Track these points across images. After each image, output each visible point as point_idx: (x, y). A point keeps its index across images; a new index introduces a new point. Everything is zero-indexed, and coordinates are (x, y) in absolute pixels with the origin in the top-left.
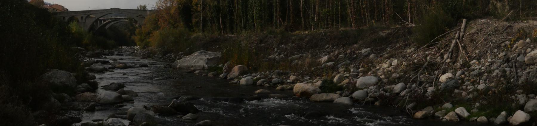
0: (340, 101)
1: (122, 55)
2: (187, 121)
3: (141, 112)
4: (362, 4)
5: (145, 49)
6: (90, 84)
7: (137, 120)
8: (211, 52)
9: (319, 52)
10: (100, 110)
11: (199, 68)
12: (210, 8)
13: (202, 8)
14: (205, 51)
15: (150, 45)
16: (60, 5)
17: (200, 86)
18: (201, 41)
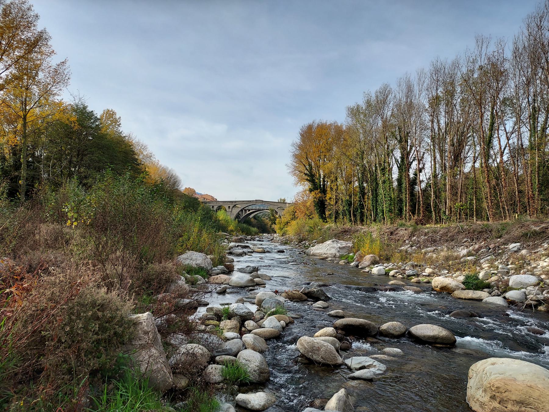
0: (491, 301)
1: (263, 241)
2: (316, 308)
3: (271, 297)
4: (500, 198)
7: (266, 306)
9: (456, 246)
10: (231, 293)
12: (342, 202)
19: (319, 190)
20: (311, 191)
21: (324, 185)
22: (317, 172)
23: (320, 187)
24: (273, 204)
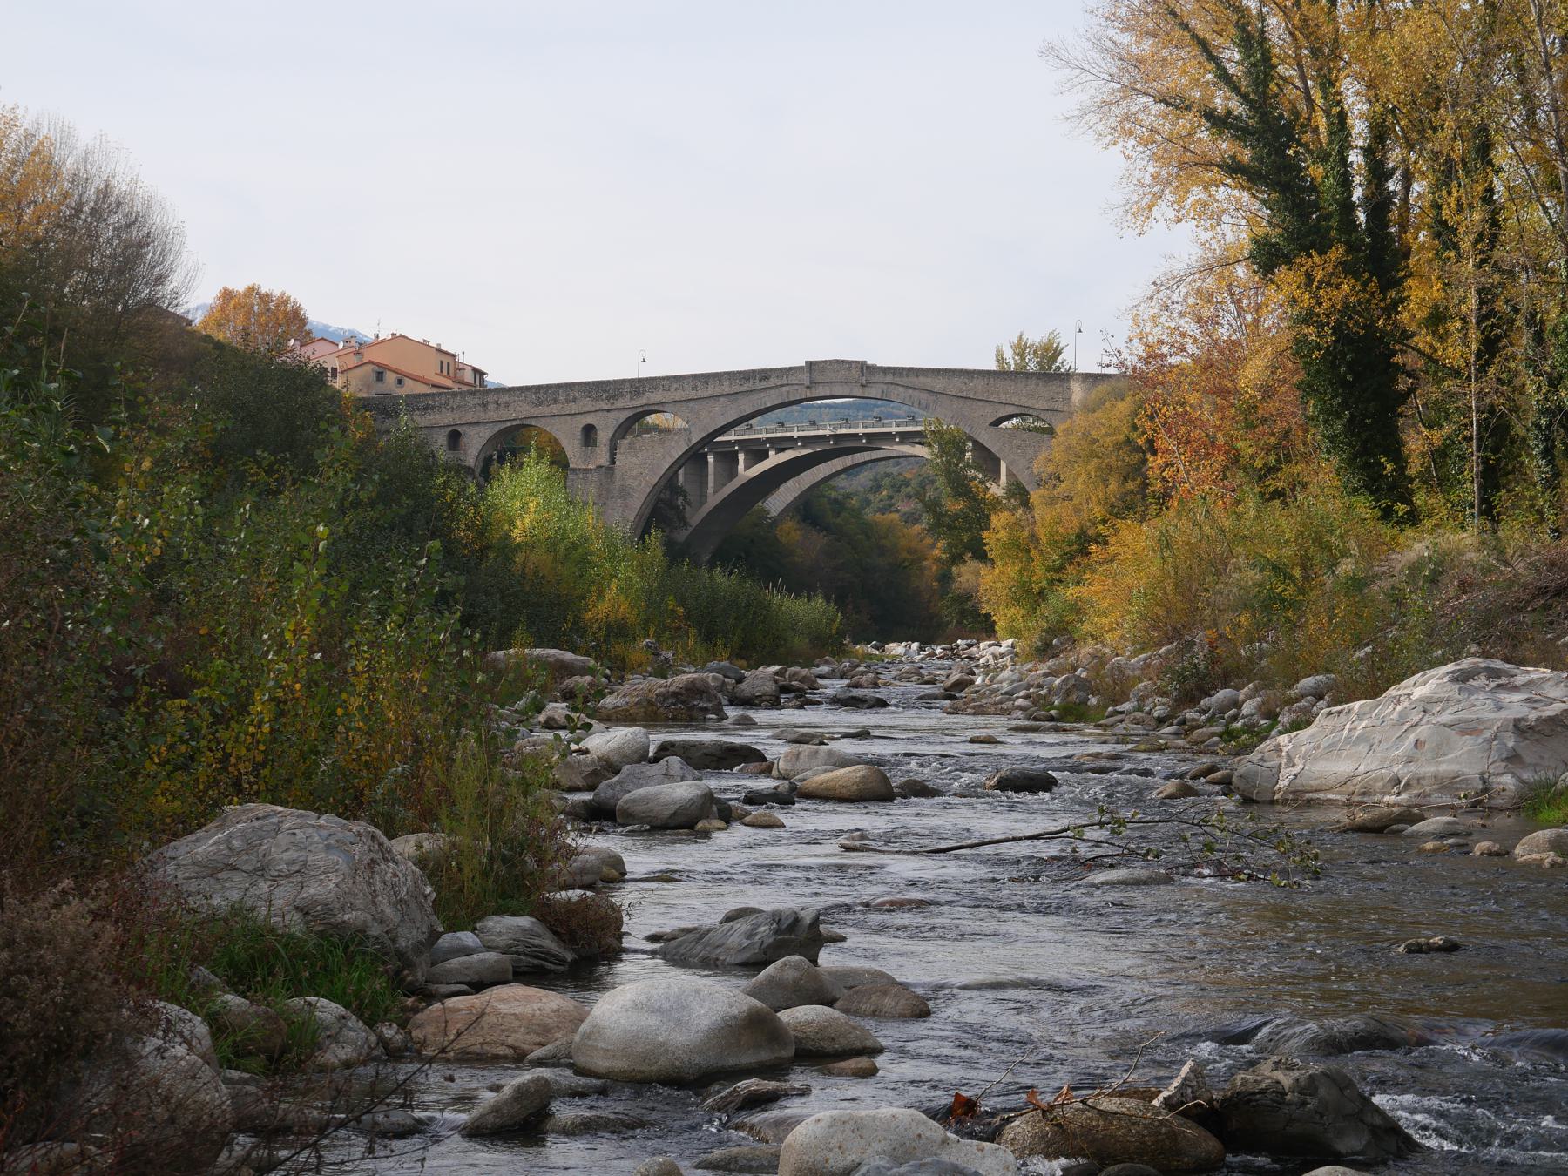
1: (881, 704)
5: (1056, 656)
6: (558, 921)
8: (1545, 672)
11: (1447, 800)
12: (1539, 339)
13: (1474, 346)
14: (1498, 664)
15: (1086, 627)
16: (425, 344)
17: (1438, 940)
18: (1464, 587)
19: (1336, 253)
20: (1267, 258)
21: (1379, 205)
22: (1317, 95)
23: (1349, 223)
24: (955, 386)
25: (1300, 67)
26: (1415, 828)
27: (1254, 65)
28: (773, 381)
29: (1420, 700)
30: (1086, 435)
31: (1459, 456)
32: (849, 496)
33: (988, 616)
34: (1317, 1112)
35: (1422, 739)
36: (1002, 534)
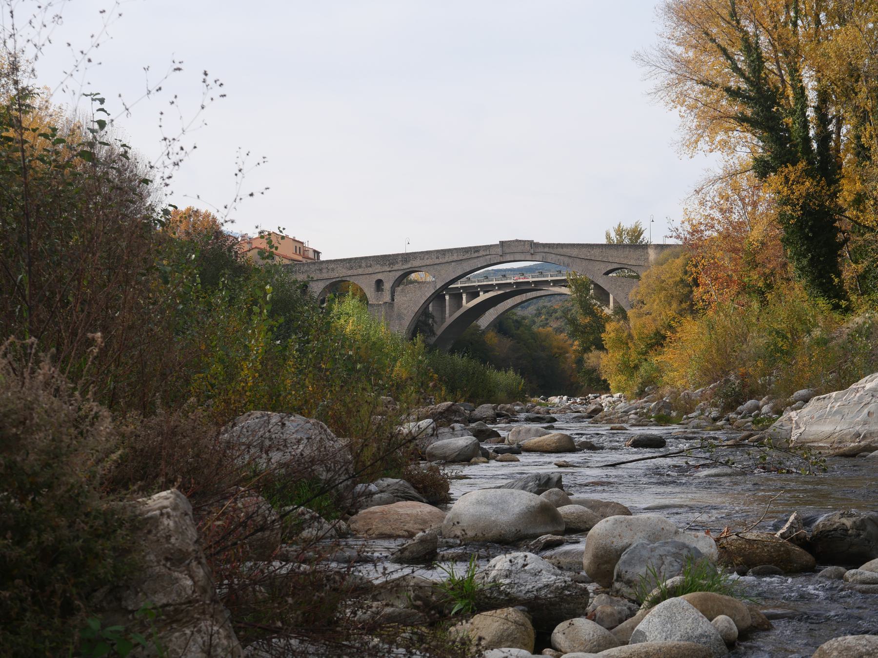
2: (865, 587)
19: (802, 165)
20: (763, 169)
21: (824, 138)
22: (787, 78)
24: (583, 253)
25: (778, 62)
26: (873, 454)
27: (752, 61)
28: (481, 253)
29: (870, 390)
30: (658, 278)
31: (874, 277)
32: (524, 318)
33: (605, 381)
34: (866, 540)
35: (872, 411)
36: (612, 335)
